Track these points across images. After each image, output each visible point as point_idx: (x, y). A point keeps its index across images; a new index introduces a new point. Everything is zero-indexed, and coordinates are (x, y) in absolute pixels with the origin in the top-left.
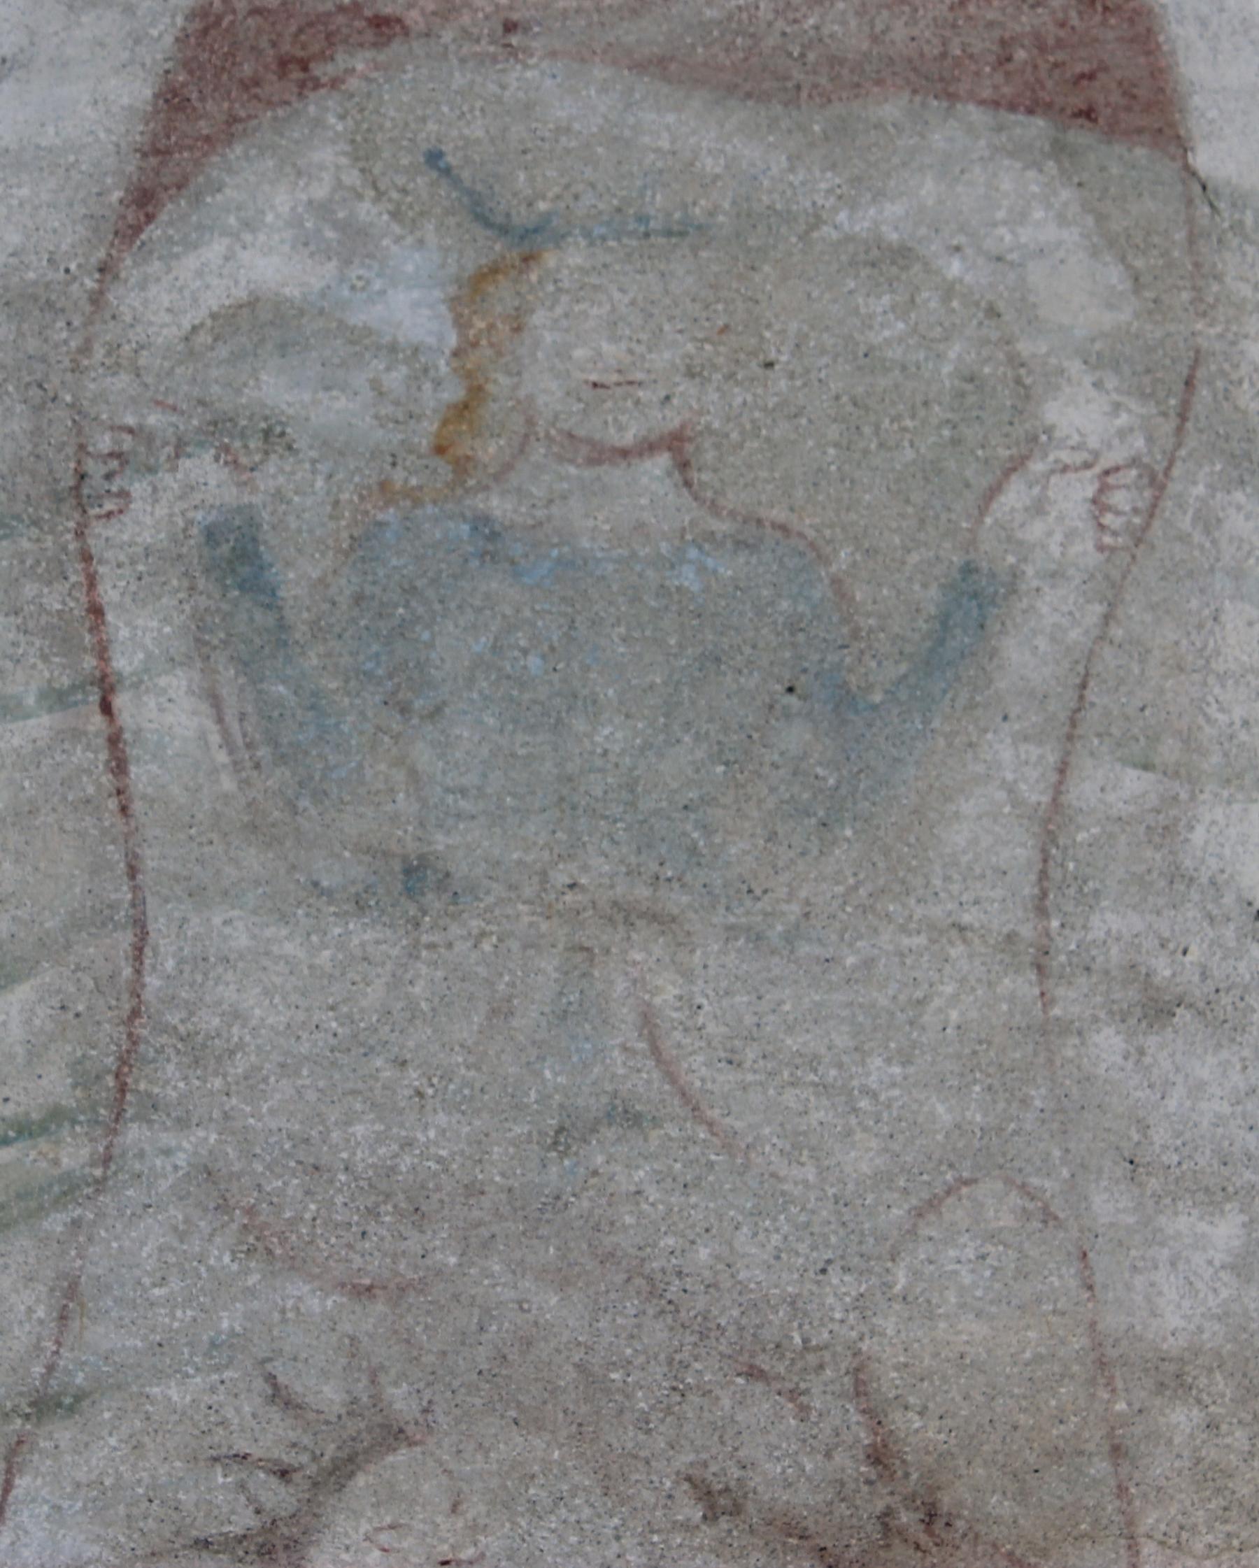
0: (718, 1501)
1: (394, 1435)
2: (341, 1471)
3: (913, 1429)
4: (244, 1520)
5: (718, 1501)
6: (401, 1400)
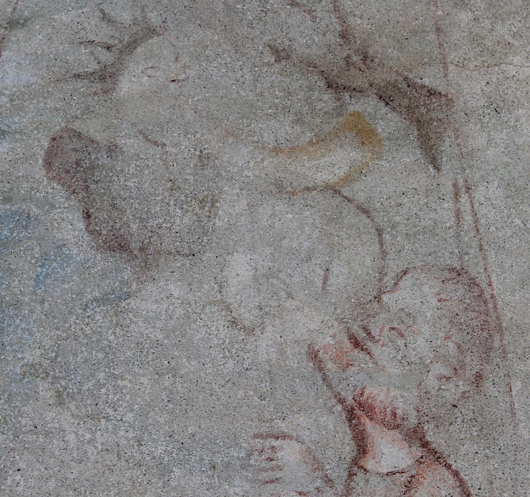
0: (281, 54)
1: (152, 32)
2: (131, 46)
3: (358, 25)
4: (93, 66)
5: (281, 54)
6: (154, 18)
